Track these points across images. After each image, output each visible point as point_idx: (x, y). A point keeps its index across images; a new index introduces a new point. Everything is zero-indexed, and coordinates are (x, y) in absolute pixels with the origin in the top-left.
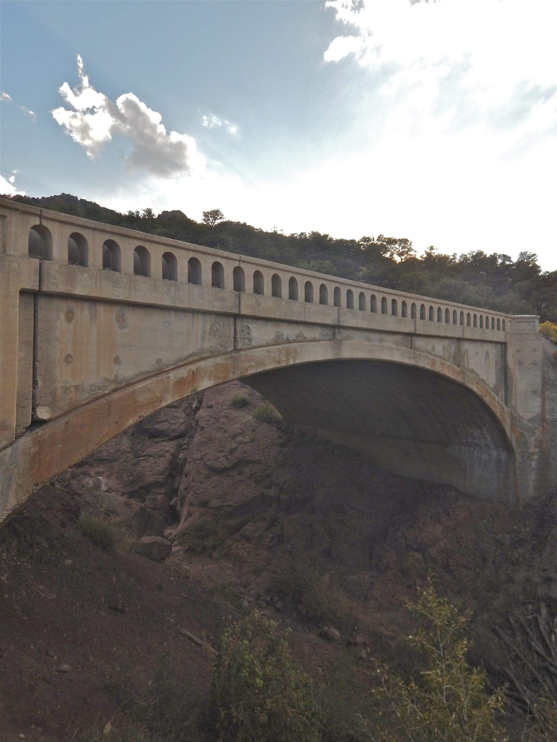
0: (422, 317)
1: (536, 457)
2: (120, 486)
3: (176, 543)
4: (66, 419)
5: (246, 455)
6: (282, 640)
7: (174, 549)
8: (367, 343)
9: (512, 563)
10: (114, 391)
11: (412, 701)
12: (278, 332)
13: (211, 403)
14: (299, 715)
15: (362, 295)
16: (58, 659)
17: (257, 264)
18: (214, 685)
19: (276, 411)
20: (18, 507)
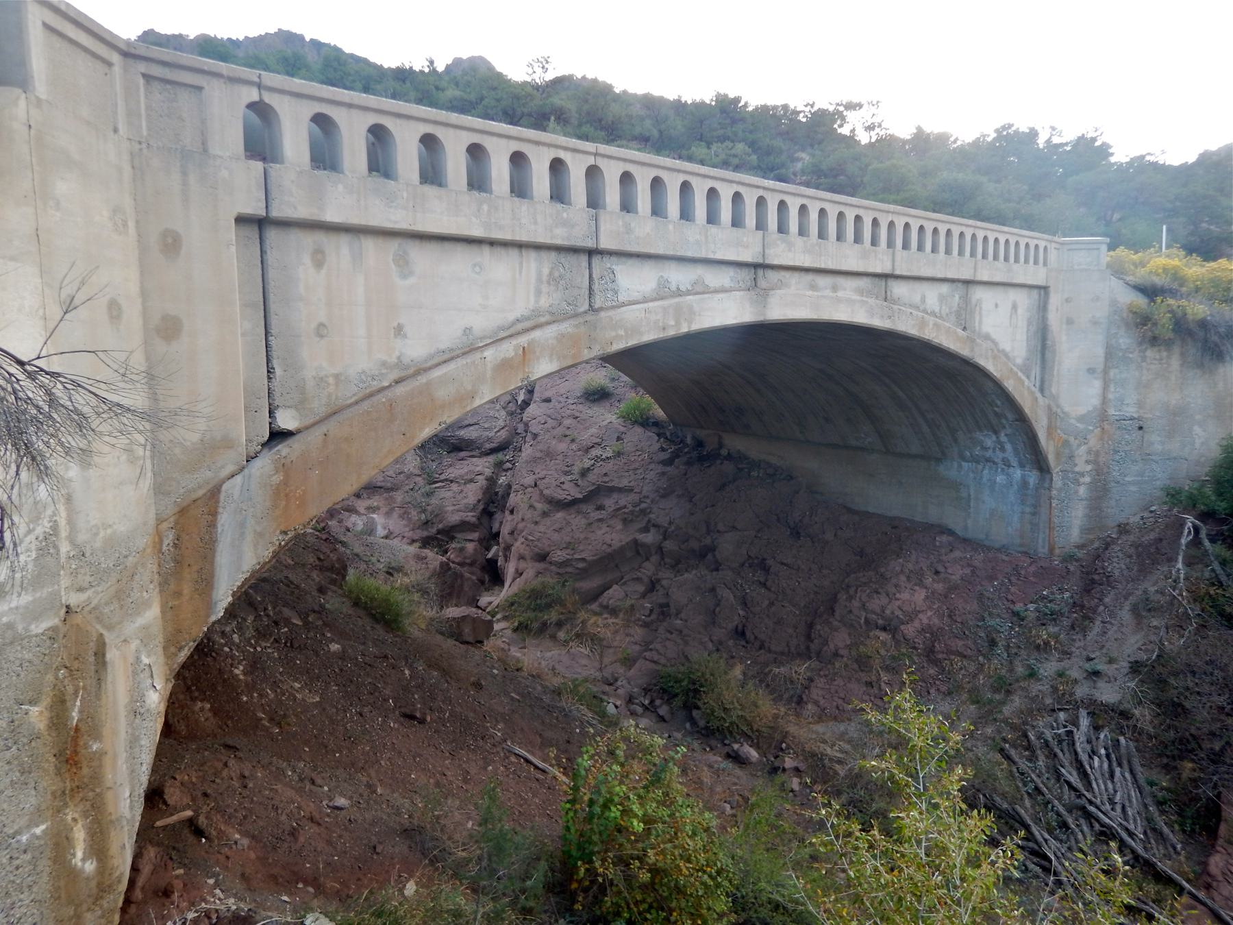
0: (906, 246)
1: (1087, 479)
2: (407, 529)
3: (499, 616)
4: (323, 428)
5: (606, 479)
6: (671, 764)
7: (497, 627)
8: (810, 293)
9: (1038, 647)
10: (398, 382)
11: (874, 857)
12: (662, 277)
13: (547, 394)
14: (698, 871)
15: (803, 209)
16: (330, 790)
17: (625, 160)
18: (568, 829)
19: (657, 406)
20: (258, 567)
